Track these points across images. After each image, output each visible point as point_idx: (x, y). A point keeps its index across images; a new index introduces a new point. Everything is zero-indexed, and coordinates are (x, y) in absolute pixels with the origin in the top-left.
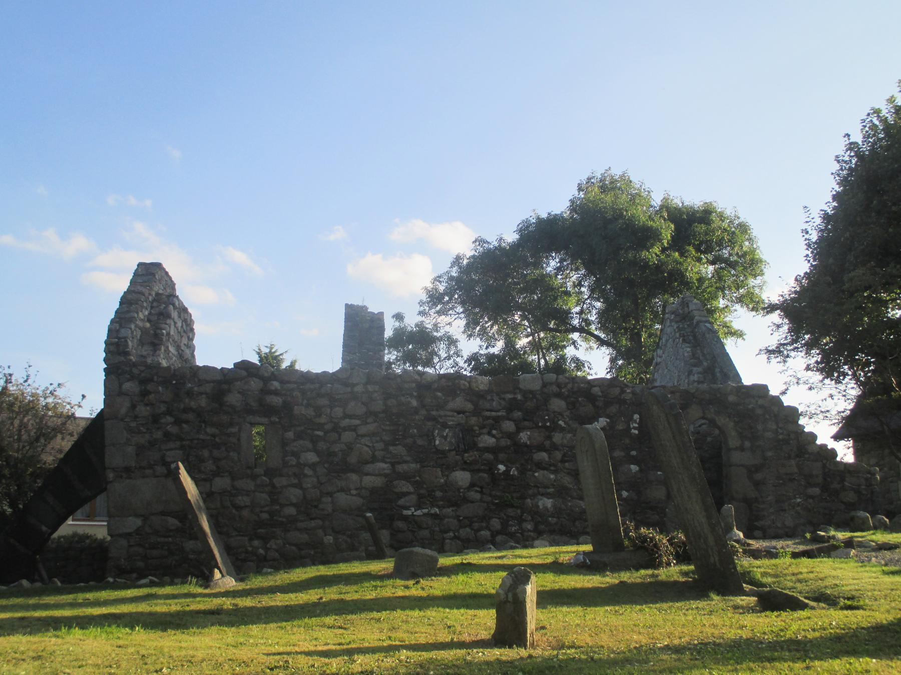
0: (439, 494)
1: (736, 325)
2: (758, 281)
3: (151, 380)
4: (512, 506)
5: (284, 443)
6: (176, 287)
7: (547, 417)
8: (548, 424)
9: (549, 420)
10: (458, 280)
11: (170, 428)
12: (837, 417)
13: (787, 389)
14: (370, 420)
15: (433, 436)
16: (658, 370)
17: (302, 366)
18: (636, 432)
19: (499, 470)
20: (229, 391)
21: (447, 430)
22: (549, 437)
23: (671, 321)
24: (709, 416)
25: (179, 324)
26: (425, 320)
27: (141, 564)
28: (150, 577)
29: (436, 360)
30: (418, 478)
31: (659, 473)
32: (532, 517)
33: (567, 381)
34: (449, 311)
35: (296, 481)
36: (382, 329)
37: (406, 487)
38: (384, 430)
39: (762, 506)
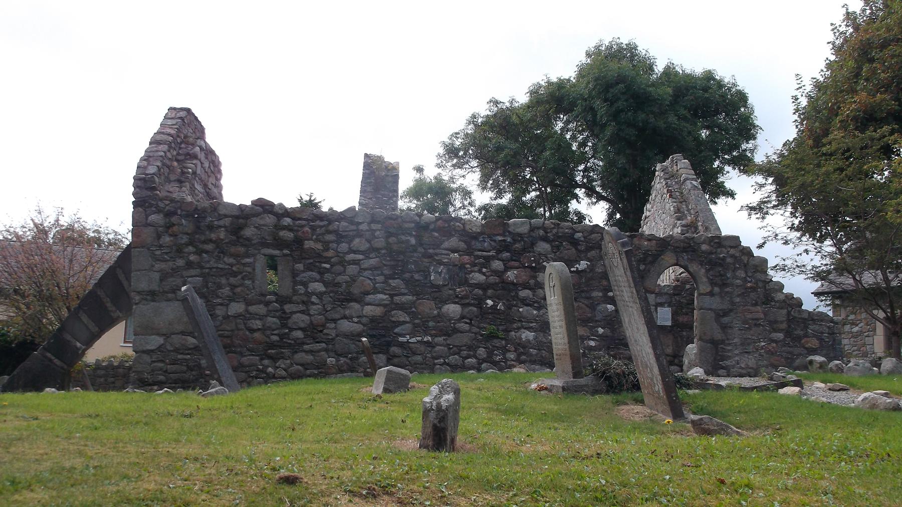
0: (431, 324)
1: (728, 185)
3: (175, 213)
4: (498, 337)
5: (295, 274)
7: (533, 259)
8: (534, 265)
9: (534, 261)
10: (473, 136)
11: (192, 258)
13: (764, 243)
19: (487, 304)
23: (661, 178)
24: (682, 264)
25: (206, 165)
26: (441, 172)
27: (161, 378)
28: (166, 389)
30: (414, 309)
33: (553, 226)
34: (464, 164)
35: (304, 308)
36: (396, 178)
37: (402, 316)
38: (385, 265)
39: (729, 348)
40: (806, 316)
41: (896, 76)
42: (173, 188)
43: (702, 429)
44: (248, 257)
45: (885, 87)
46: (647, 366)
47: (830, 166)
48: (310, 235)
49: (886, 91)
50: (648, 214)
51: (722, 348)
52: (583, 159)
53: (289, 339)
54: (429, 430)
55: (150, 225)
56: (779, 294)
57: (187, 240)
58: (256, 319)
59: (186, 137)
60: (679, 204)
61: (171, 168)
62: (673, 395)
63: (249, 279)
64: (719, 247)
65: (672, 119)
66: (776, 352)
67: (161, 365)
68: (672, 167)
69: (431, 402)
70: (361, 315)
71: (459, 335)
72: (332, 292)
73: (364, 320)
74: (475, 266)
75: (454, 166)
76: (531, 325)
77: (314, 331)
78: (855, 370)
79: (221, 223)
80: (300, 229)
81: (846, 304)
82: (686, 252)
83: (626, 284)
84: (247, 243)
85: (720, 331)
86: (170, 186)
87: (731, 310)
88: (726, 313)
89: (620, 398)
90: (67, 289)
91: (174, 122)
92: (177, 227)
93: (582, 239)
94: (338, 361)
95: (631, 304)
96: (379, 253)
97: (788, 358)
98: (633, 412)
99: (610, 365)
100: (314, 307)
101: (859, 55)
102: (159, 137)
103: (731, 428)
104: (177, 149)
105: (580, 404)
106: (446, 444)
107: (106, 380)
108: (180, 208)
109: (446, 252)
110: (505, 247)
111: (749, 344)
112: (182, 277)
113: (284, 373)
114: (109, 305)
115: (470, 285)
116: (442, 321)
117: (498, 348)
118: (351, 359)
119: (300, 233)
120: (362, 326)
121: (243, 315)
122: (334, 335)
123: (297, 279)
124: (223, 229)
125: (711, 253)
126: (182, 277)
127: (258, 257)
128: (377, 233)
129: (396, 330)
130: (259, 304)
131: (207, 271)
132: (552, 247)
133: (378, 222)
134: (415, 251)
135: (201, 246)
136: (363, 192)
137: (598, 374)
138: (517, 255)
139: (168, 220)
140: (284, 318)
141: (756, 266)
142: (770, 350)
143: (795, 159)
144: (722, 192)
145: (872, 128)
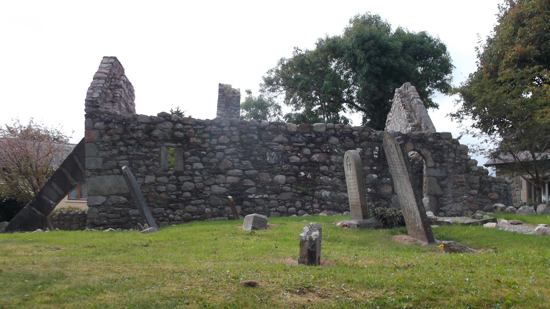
0: (268, 187)
1: (434, 101)
2: (448, 77)
3: (111, 122)
4: (308, 195)
5: (185, 158)
6: (125, 71)
8: (329, 151)
11: (122, 149)
12: (489, 153)
13: (461, 136)
14: (231, 146)
15: (266, 156)
16: (389, 124)
17: (196, 116)
18: (377, 156)
19: (301, 175)
20: (155, 129)
21: (274, 153)
22: (329, 158)
24: (417, 149)
25: (127, 91)
27: (105, 221)
28: (110, 229)
29: (268, 116)
30: (257, 178)
31: (388, 179)
32: (318, 201)
33: (340, 127)
36: (239, 97)
37: (250, 183)
38: (239, 152)
39: (445, 199)
40: (490, 179)
41: (538, 35)
42: (109, 106)
43: (449, 249)
44: (156, 147)
45: (532, 41)
46: (411, 212)
47: (501, 89)
48: (194, 134)
49: (533, 44)
50: (390, 119)
51: (441, 199)
52: (347, 85)
53: (182, 197)
54: (305, 253)
55: (95, 129)
56: (475, 167)
57: (119, 138)
58: (161, 185)
59: (114, 74)
60: (410, 113)
61: (107, 94)
62: (428, 229)
63: (158, 161)
64: (439, 139)
65: (403, 61)
66: (473, 201)
67: (104, 214)
68: (405, 90)
69: (305, 236)
70: (225, 182)
71: (284, 193)
72: (207, 168)
73: (227, 185)
74: (293, 152)
75: (270, 90)
76: (328, 187)
77: (197, 192)
78: (523, 212)
79: (140, 127)
80: (187, 130)
81: (504, 171)
82: (419, 142)
83: (400, 164)
84: (156, 139)
85: (440, 189)
86: (107, 105)
87: (446, 177)
88: (443, 179)
89: (393, 230)
90: (36, 168)
91: (107, 65)
92: (112, 130)
93: (358, 135)
94: (212, 210)
95: (402, 175)
96: (236, 145)
97: (480, 205)
98: (402, 239)
99: (385, 211)
100: (197, 178)
101: (516, 22)
102: (99, 75)
103: (468, 249)
104: (110, 82)
105: (371, 234)
106: (316, 261)
107: (59, 223)
108: (114, 118)
109: (276, 144)
110: (311, 140)
111: (457, 197)
112: (116, 160)
113: (179, 218)
114: (70, 177)
115: (291, 164)
116: (275, 185)
117: (308, 201)
118: (220, 209)
119: (187, 133)
120: (226, 189)
121: (153, 183)
122: (209, 195)
123: (186, 161)
124: (140, 131)
125: (434, 143)
126: (116, 160)
127: (162, 148)
128: (234, 133)
129: (247, 191)
130: (164, 176)
131: (131, 156)
132: (339, 140)
133: (235, 126)
134: (257, 143)
135: (127, 141)
136: (219, 107)
137: (378, 217)
138: (318, 145)
139: (107, 126)
140: (179, 184)
141: (461, 151)
142: (469, 200)
143: (480, 85)
144: (430, 104)
145: (527, 67)
